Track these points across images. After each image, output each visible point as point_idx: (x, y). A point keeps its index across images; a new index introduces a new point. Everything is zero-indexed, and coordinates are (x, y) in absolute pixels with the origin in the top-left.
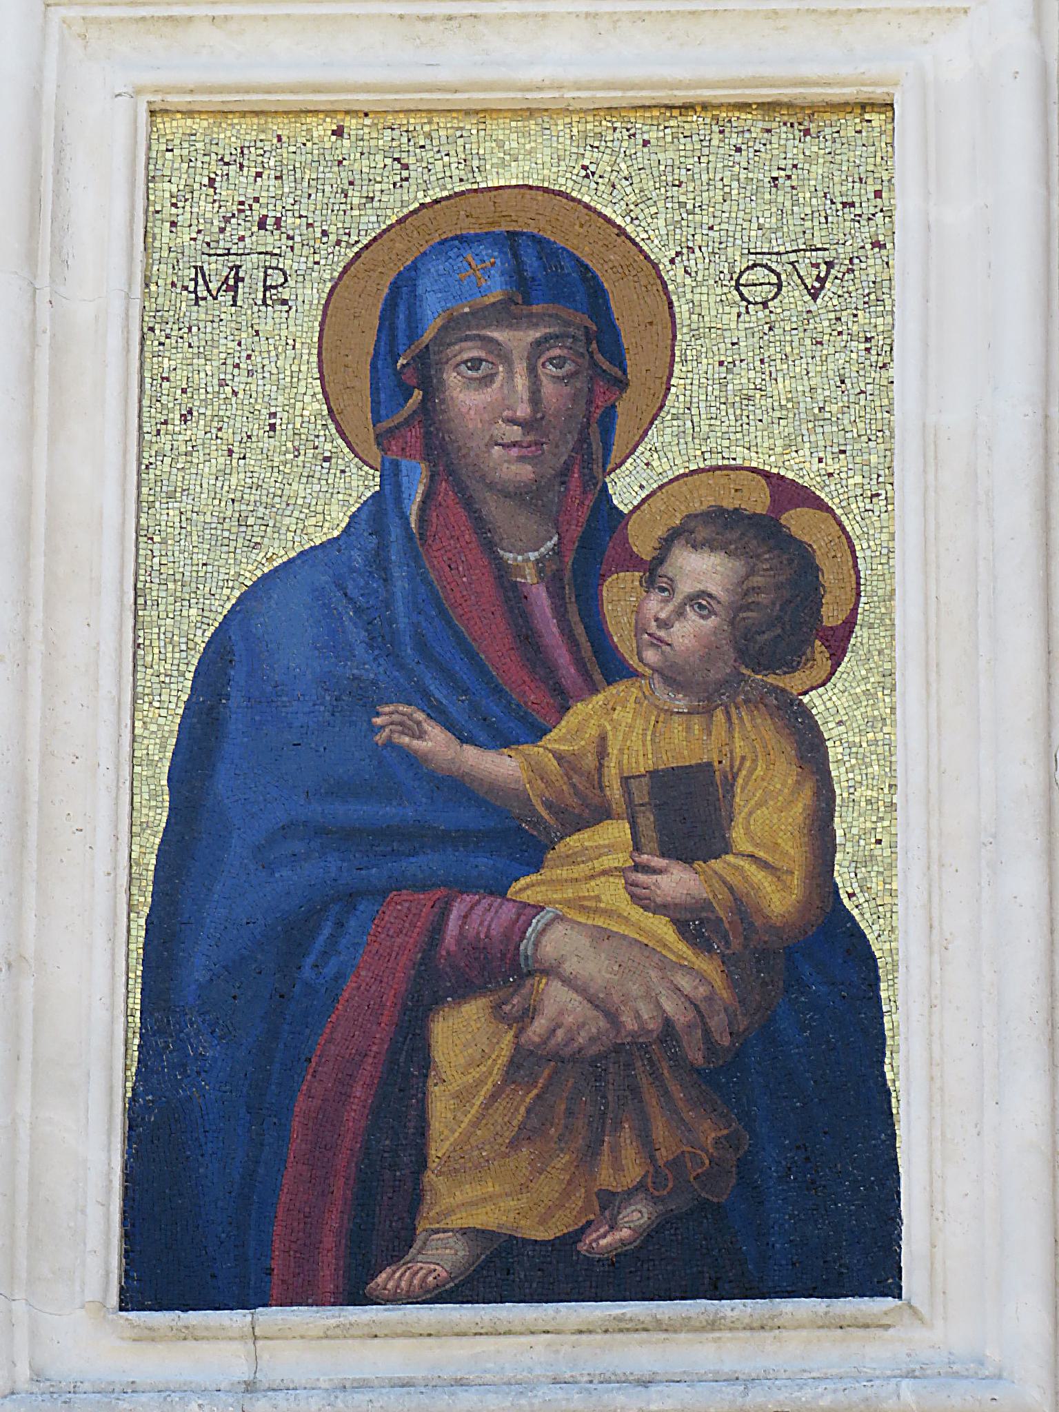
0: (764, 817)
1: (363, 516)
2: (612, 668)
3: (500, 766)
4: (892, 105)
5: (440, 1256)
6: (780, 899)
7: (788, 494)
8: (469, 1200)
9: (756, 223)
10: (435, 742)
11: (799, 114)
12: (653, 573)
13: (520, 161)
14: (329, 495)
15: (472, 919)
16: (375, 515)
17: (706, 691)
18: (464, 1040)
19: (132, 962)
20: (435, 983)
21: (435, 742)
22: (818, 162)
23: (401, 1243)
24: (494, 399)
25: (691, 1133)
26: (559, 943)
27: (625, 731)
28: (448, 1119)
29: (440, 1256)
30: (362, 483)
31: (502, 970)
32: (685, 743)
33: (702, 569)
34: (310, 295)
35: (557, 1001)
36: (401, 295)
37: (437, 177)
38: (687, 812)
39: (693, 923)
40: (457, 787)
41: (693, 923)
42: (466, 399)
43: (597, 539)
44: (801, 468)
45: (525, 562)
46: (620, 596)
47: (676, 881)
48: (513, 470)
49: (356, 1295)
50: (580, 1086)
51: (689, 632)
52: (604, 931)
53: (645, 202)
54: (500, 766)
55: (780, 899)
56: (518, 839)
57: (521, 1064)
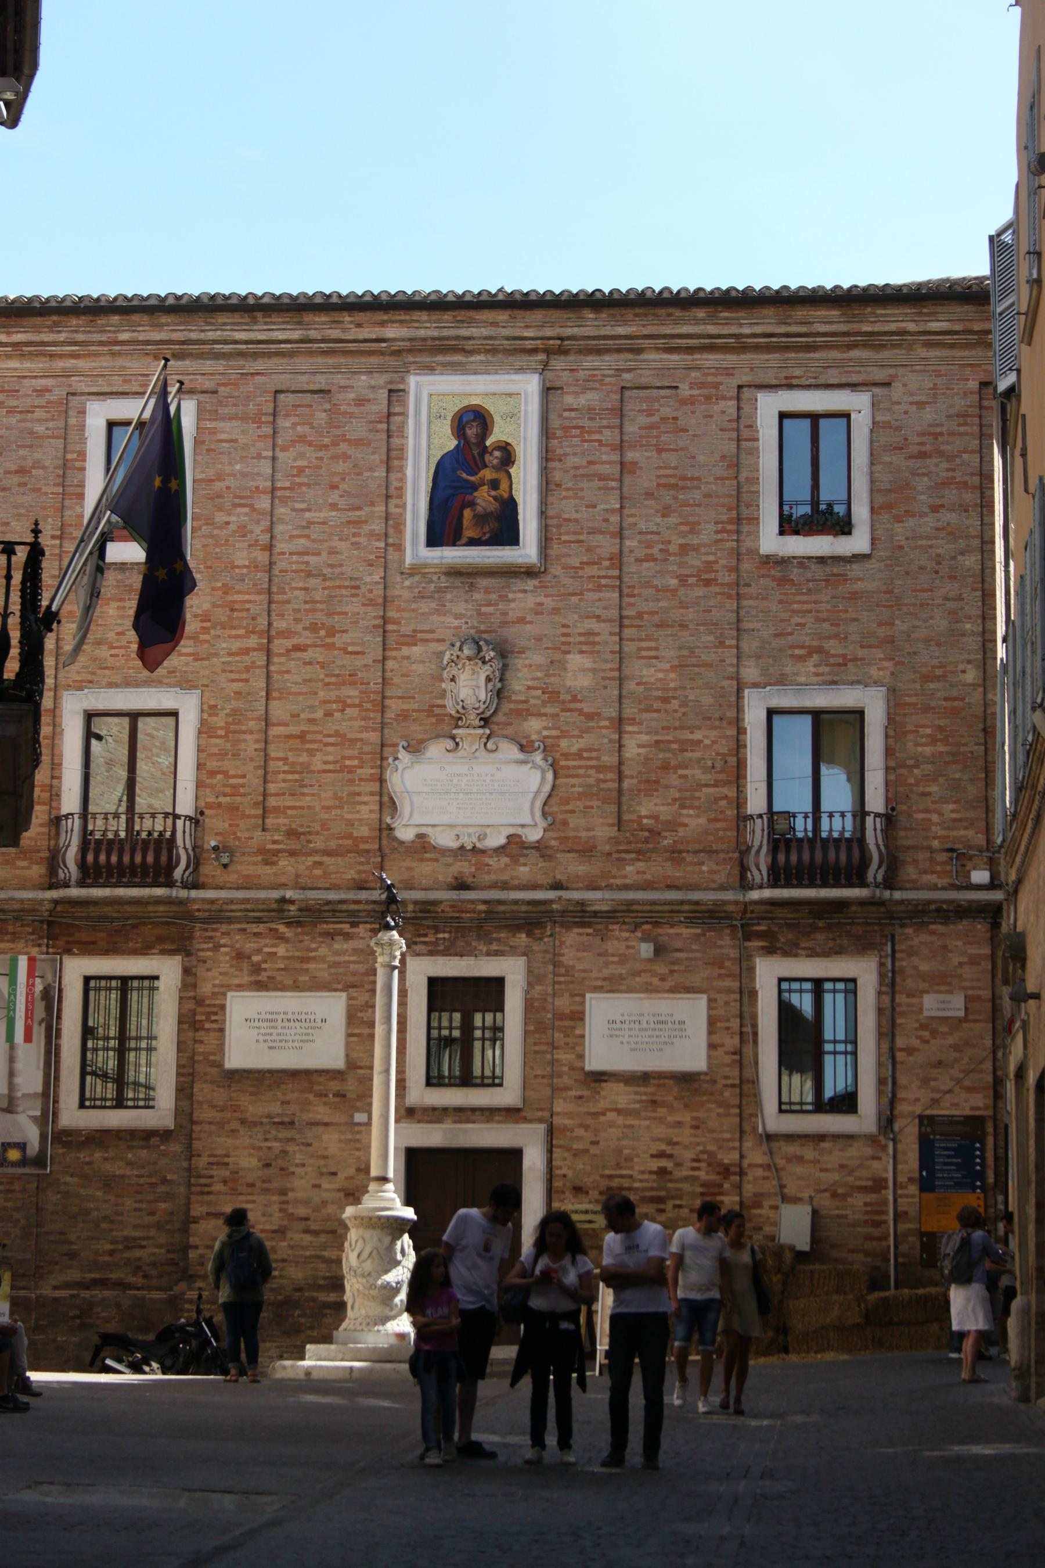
0: (504, 485)
1: (624, 988)
2: (486, 466)
3: (472, 478)
4: (781, 1111)
5: (464, 540)
6: (506, 495)
7: (508, 444)
8: (468, 533)
9: (504, 409)
10: (464, 475)
11: (510, 395)
12: (491, 454)
13: (475, 401)
14: (452, 444)
15: (468, 498)
16: (457, 446)
17: (497, 469)
18: (467, 513)
19: (617, 1180)
20: (464, 505)
21: (464, 475)
22: (512, 401)
23: (459, 539)
24: (471, 432)
25: (494, 525)
26: (479, 501)
27: (487, 474)
28: (466, 523)
29: (464, 540)
30: (455, 442)
31: (472, 504)
32: (495, 476)
33: (497, 454)
34: (449, 418)
35: (479, 508)
36: (461, 418)
37: (466, 403)
38: (495, 484)
39: (495, 498)
40: (467, 481)
41: (495, 498)
42: (469, 432)
43: (484, 450)
44: (509, 441)
45: (475, 452)
46: (487, 457)
47: (493, 493)
48: (474, 441)
49: (454, 545)
50: (481, 519)
51: (495, 462)
52: (484, 498)
53: (491, 406)
54: (472, 478)
55: (506, 495)
56: (475, 487)
57: (475, 516)
